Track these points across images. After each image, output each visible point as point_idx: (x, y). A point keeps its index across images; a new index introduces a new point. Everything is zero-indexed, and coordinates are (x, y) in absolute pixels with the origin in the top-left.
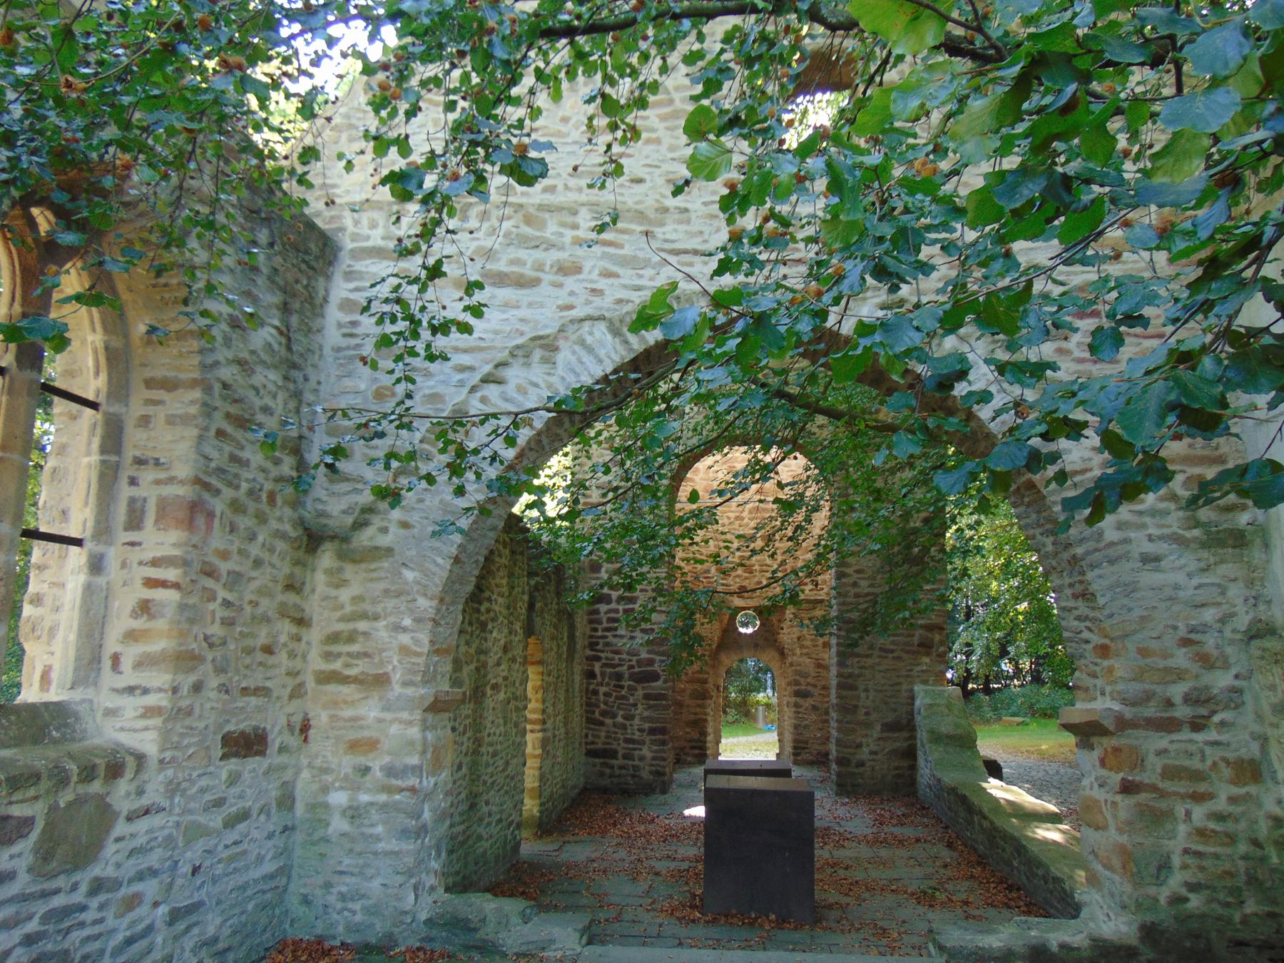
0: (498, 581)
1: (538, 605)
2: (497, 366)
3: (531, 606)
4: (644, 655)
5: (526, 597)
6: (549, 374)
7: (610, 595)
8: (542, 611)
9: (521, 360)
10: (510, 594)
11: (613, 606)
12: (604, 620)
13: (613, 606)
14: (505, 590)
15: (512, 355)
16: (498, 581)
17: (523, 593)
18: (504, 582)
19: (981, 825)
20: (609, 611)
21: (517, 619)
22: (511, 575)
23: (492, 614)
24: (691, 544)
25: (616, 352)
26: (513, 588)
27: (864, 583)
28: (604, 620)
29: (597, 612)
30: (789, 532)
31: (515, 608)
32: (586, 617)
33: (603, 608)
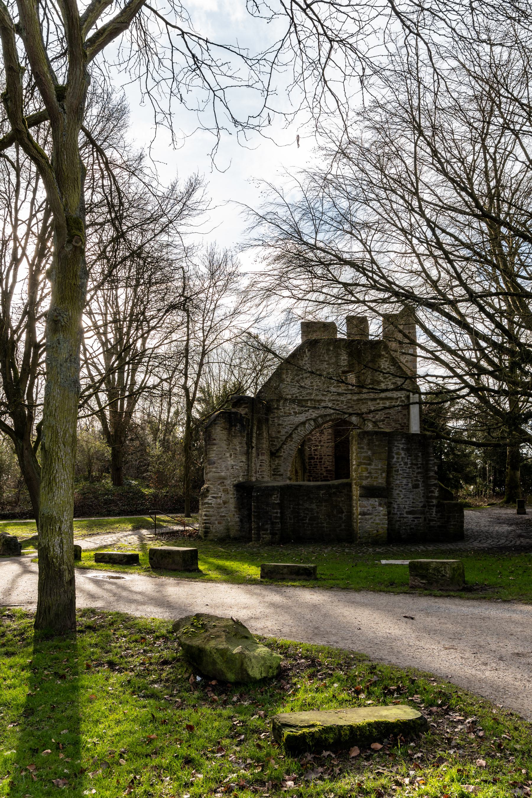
4: (325, 474)
33: (312, 461)
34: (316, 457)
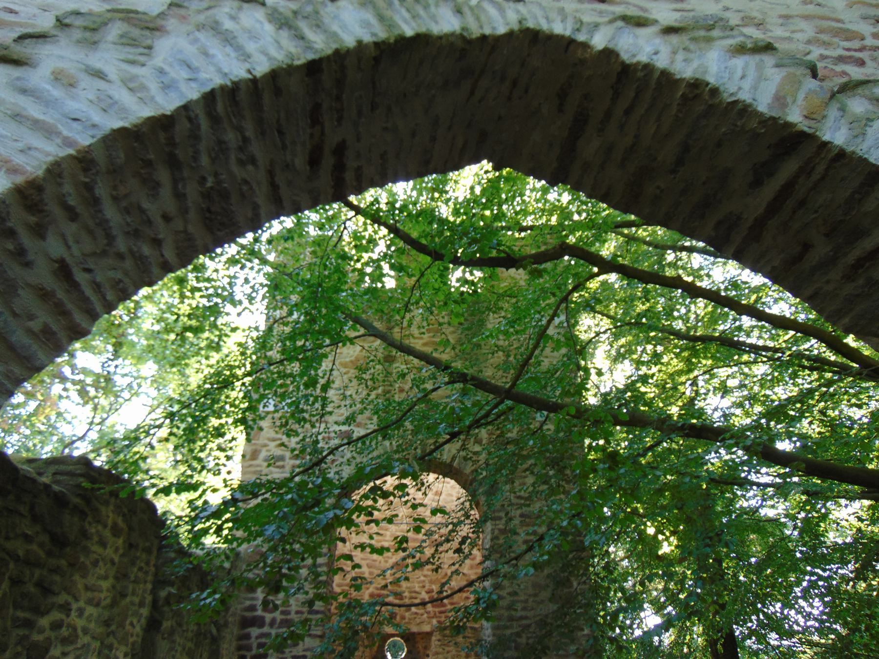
0: (91, 580)
1: (166, 624)
2: (22, 38)
3: (153, 625)
5: (145, 612)
6: (133, 63)
7: (263, 618)
8: (172, 632)
9: (78, 34)
10: (114, 604)
11: (266, 629)
12: (255, 645)
13: (266, 629)
14: (105, 597)
15: (61, 23)
16: (91, 580)
17: (142, 604)
18: (105, 585)
19: (205, 532)
20: (262, 635)
21: (123, 641)
22: (122, 576)
23: (64, 632)
24: (368, 523)
25: (280, 47)
26: (124, 596)
27: (519, 606)
28: (255, 645)
29: (248, 636)
30: (455, 545)
31: (121, 625)
32: (234, 644)
33: (255, 632)
34: (268, 617)
